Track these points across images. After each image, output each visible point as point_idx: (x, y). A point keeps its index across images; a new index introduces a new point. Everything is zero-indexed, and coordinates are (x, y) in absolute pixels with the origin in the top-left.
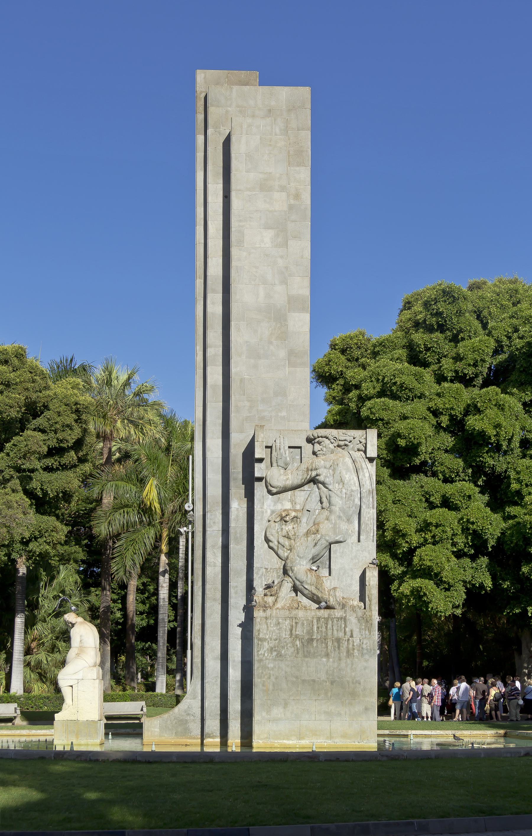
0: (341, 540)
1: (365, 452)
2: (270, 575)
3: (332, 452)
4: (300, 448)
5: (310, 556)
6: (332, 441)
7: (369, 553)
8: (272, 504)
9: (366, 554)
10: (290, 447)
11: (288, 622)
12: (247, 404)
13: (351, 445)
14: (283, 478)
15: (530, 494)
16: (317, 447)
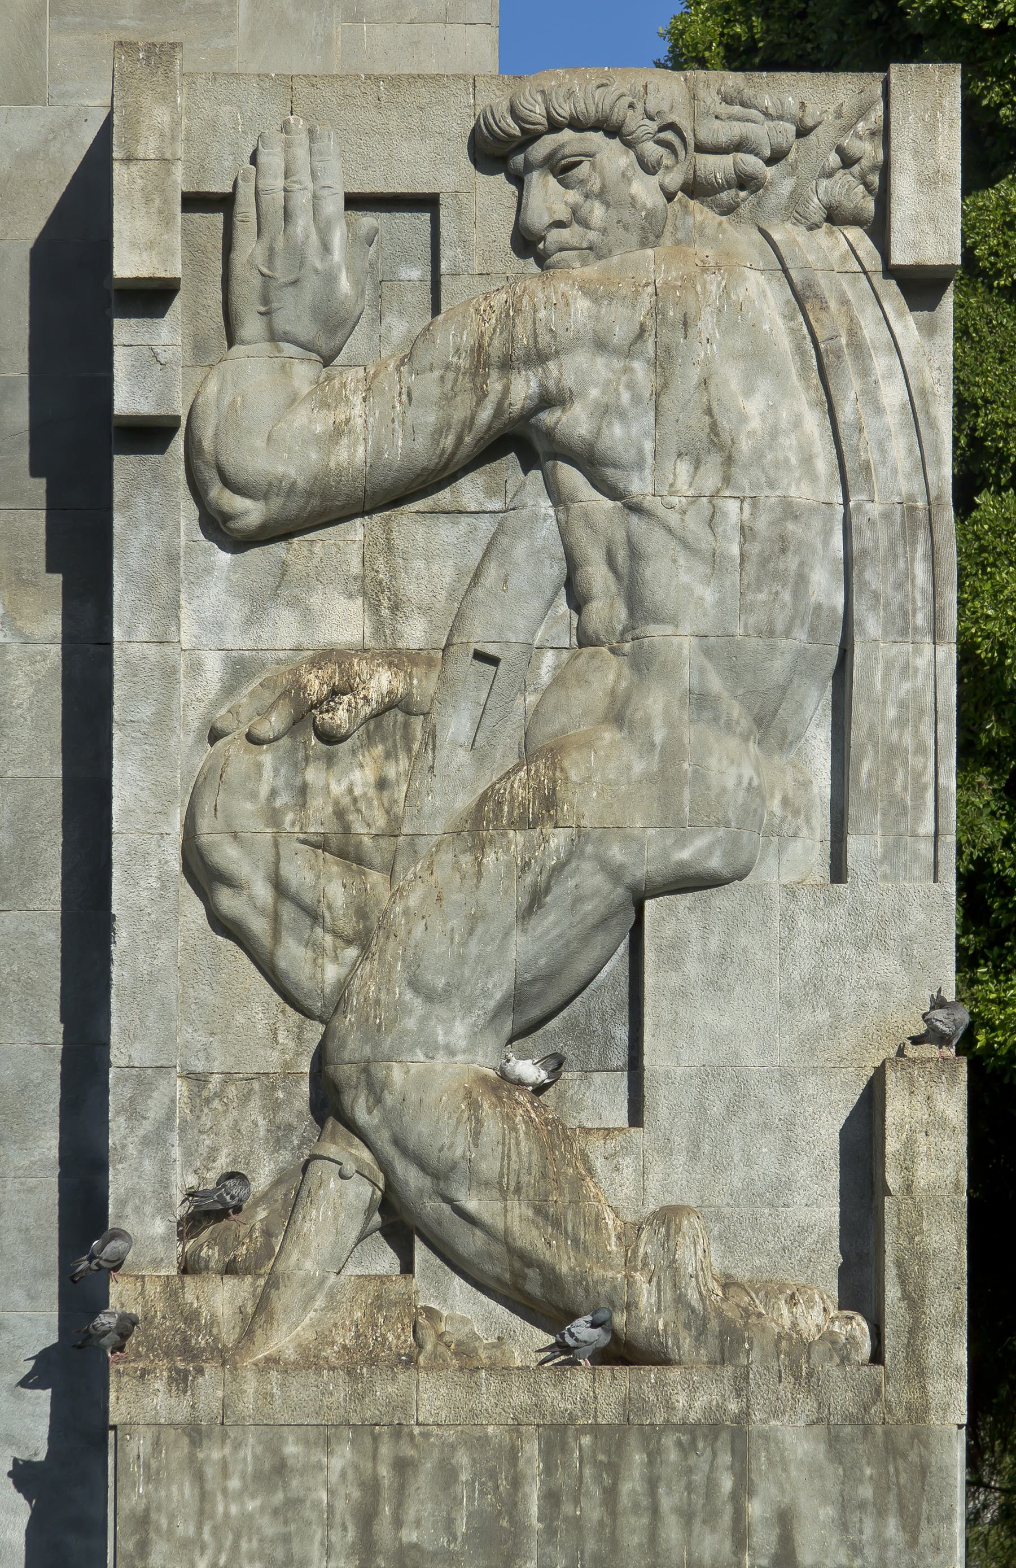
0: (715, 863)
1: (880, 230)
2: (225, 1124)
4: (427, 203)
5: (499, 985)
6: (651, 150)
7: (907, 959)
9: (885, 965)
10: (355, 202)
14: (309, 421)
16: (547, 198)
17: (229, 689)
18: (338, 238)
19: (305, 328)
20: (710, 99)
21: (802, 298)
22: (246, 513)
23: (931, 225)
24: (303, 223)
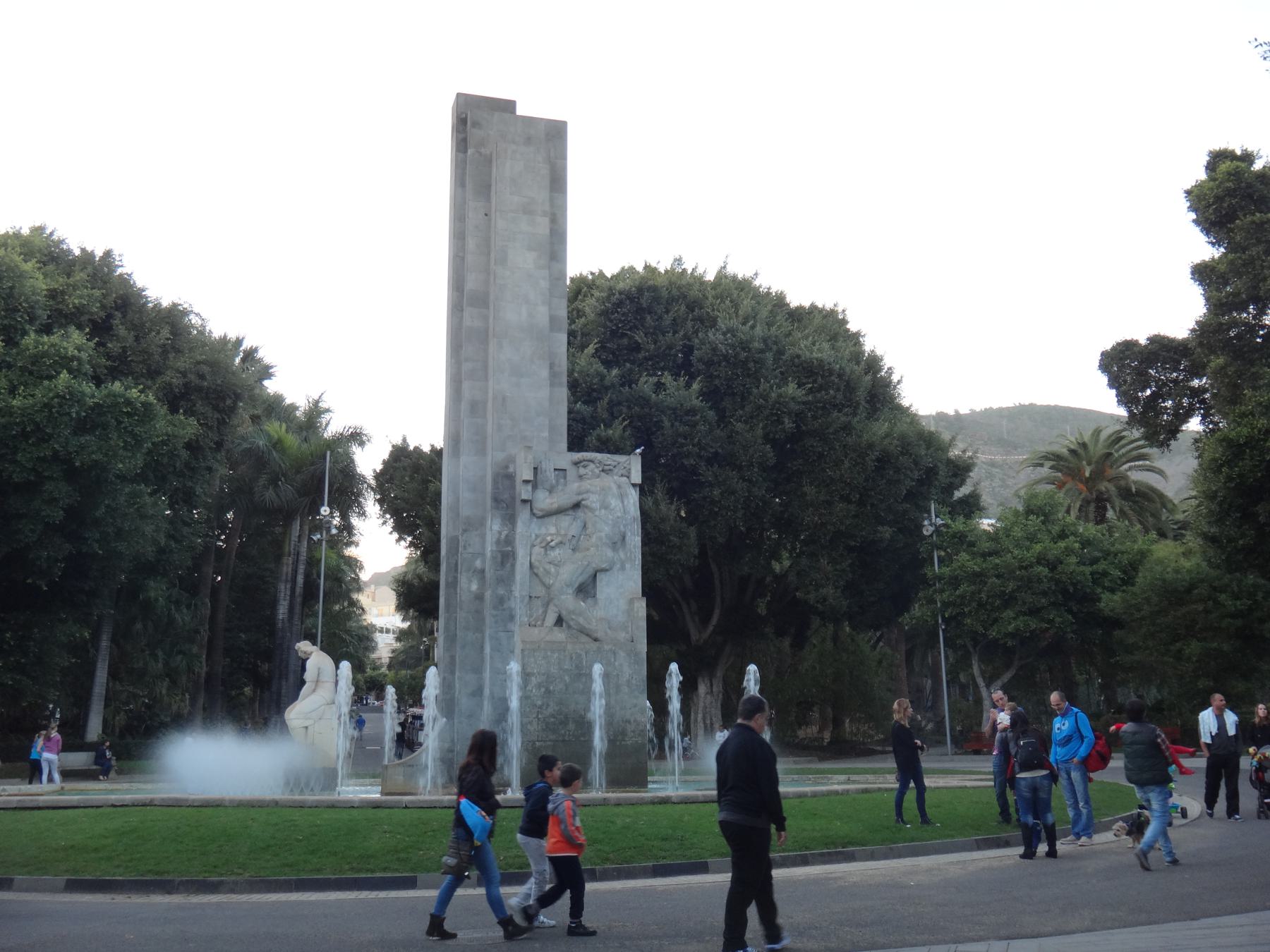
13: (616, 470)
16: (582, 471)
21: (619, 487)
23: (637, 477)
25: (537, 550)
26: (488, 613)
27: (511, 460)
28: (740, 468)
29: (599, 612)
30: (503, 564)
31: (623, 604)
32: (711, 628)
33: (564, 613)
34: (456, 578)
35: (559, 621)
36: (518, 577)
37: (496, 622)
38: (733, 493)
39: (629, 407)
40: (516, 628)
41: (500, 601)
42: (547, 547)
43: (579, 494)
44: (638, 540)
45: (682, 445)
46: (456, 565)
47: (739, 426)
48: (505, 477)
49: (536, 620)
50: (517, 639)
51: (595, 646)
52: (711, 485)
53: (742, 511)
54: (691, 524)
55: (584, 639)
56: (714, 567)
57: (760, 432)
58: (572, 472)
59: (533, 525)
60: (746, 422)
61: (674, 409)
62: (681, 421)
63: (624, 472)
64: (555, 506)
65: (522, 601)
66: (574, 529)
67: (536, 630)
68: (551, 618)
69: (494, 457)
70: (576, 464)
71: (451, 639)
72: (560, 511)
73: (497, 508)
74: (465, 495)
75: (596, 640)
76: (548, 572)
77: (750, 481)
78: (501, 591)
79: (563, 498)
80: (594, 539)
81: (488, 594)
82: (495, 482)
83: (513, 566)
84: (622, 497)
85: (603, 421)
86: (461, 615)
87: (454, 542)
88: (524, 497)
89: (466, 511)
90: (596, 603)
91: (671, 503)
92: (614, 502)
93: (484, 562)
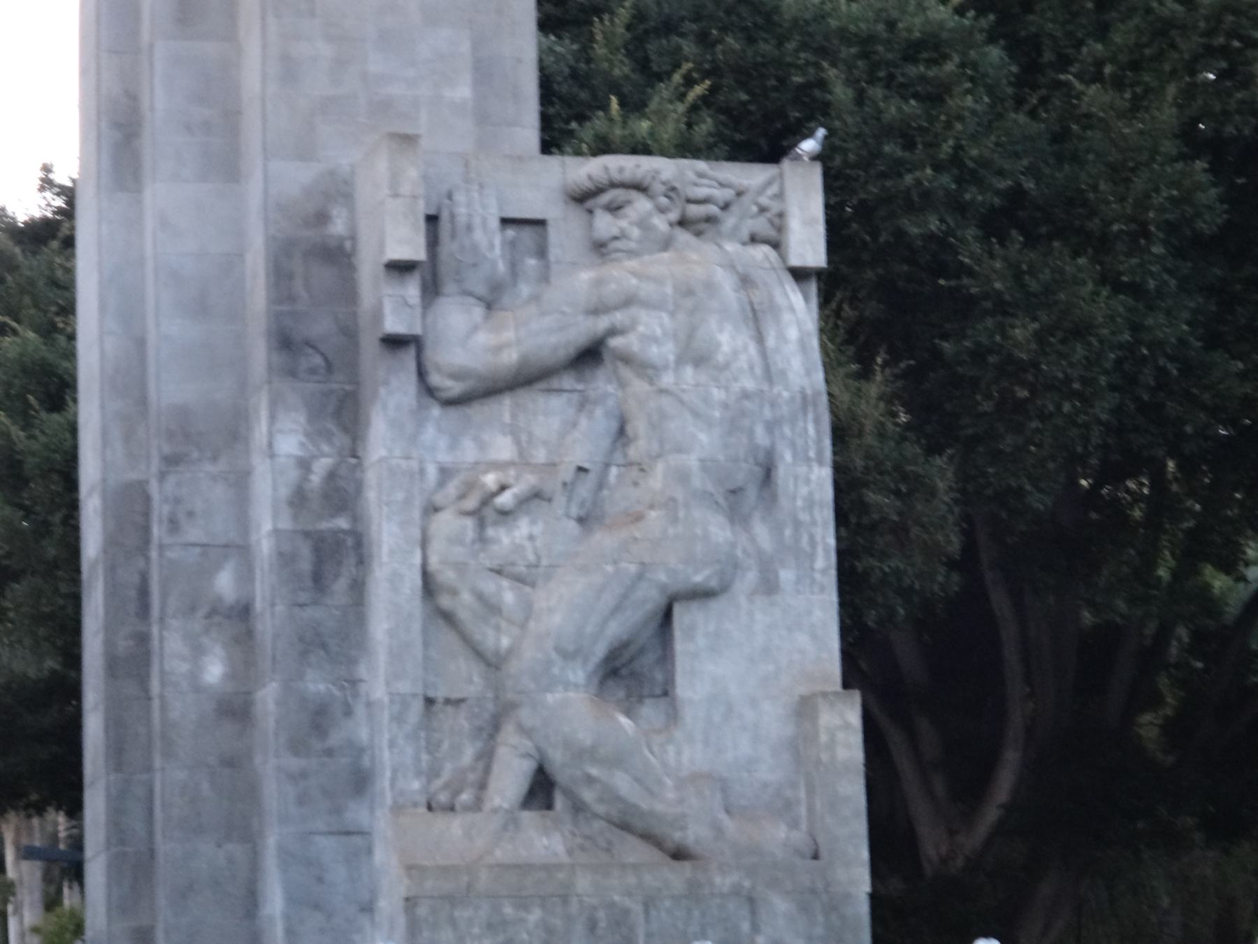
0: (714, 583)
3: (666, 244)
4: (541, 223)
5: (600, 651)
6: (663, 201)
7: (814, 636)
8: (443, 443)
9: (803, 639)
10: (506, 222)
11: (535, 916)
12: (325, 50)
13: (730, 221)
14: (483, 338)
15: (921, 8)
16: (605, 224)
17: (441, 484)
18: (497, 241)
19: (481, 290)
20: (691, 176)
21: (745, 281)
22: (449, 389)
23: (809, 248)
24: (478, 235)
25: (447, 523)
26: (272, 766)
27: (339, 190)
28: (1101, 245)
29: (687, 753)
30: (319, 580)
31: (774, 720)
32: (991, 815)
33: (557, 758)
34: (143, 639)
35: (541, 789)
36: (380, 627)
37: (302, 800)
38: (1080, 331)
39: (703, 39)
40: (382, 823)
41: (318, 720)
42: (486, 512)
43: (596, 311)
44: (821, 479)
45: (897, 168)
46: (144, 592)
47: (1094, 97)
48: (316, 254)
49: (455, 788)
50: (385, 857)
51: (676, 877)
52: (1002, 308)
53: (1113, 399)
54: (933, 450)
55: (635, 851)
56: (1000, 601)
57: (1167, 114)
58: (566, 232)
59: (430, 432)
60: (1118, 83)
61: (866, 42)
62: (889, 82)
63: (761, 225)
64: (510, 358)
65: (398, 719)
66: (586, 443)
67: (455, 826)
68: (510, 779)
69: (274, 179)
70: (582, 198)
71: (137, 869)
72: (528, 378)
73: (292, 373)
74: (168, 329)
75: (679, 854)
76: (490, 607)
77: (1135, 290)
78: (316, 684)
79: (538, 326)
80: (657, 480)
81: (268, 697)
82: (280, 275)
83: (358, 588)
84: (756, 318)
85: (615, 87)
86: (169, 778)
87: (132, 507)
88: (394, 324)
89: (171, 389)
90: (673, 716)
91: (865, 374)
92: (729, 339)
93: (246, 575)
